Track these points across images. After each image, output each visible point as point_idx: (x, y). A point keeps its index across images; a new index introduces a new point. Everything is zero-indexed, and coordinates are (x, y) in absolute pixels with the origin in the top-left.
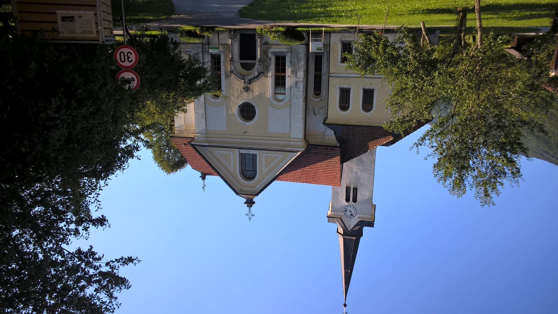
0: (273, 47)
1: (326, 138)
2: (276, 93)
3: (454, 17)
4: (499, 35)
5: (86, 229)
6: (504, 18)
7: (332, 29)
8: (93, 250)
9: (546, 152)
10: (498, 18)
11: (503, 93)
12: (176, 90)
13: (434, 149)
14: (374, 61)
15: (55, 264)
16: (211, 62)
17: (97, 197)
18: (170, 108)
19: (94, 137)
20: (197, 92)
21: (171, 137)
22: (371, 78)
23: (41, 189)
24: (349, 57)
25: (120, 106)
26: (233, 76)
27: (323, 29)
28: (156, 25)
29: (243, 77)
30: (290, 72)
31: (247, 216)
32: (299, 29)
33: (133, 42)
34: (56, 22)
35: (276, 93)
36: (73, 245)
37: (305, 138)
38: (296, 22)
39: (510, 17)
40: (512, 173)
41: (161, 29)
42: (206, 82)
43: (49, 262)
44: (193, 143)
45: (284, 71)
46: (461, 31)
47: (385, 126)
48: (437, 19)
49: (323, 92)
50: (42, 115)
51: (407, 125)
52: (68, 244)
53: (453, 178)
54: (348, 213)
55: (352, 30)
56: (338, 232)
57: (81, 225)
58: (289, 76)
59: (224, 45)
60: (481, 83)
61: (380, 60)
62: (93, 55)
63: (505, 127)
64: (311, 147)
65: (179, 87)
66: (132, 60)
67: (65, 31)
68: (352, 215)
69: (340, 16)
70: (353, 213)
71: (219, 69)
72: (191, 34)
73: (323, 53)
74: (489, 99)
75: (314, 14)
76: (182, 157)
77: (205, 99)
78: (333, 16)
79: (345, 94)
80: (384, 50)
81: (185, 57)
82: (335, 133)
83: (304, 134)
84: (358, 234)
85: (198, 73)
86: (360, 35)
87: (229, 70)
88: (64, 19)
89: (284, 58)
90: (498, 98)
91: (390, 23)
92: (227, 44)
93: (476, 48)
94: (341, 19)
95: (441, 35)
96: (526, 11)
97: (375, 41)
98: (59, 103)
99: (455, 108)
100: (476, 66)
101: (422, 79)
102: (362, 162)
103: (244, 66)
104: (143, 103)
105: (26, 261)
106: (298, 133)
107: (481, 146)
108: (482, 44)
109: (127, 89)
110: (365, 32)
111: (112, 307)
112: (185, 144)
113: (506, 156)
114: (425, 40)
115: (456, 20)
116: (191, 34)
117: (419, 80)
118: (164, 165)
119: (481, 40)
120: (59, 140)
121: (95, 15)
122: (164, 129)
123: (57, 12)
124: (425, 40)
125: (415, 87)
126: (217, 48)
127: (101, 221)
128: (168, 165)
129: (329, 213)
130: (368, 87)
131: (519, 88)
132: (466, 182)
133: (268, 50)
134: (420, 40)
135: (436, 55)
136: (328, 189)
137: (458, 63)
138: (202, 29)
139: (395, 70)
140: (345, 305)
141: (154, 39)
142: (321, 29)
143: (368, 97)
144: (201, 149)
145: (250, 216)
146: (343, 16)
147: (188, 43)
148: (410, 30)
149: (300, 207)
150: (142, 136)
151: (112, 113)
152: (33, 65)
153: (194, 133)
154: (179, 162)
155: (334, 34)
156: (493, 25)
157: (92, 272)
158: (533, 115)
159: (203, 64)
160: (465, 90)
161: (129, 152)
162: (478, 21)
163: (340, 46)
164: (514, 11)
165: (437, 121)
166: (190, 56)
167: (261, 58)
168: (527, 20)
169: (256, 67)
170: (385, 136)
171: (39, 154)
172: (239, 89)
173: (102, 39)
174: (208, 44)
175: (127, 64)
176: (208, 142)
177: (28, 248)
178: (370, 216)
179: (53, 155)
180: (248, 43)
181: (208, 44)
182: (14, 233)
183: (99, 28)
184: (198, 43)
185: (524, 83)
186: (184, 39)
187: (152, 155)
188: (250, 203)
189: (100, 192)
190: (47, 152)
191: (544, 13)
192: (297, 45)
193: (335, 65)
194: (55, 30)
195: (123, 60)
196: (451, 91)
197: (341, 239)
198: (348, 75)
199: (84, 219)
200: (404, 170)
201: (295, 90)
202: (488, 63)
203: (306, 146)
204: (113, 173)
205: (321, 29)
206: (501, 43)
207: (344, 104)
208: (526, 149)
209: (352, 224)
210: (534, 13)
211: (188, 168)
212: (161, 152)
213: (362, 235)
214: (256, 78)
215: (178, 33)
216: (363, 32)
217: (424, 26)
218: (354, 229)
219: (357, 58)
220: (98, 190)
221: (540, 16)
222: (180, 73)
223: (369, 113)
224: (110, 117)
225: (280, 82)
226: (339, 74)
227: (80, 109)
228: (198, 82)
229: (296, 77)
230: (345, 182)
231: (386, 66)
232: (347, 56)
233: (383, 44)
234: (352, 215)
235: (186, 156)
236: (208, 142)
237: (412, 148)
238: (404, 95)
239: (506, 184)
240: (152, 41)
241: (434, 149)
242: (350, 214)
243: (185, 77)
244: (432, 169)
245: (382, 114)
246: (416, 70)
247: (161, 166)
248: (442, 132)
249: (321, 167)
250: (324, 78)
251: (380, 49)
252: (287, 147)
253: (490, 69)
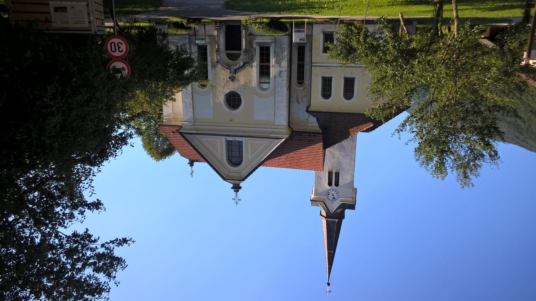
0: (258, 38)
1: (309, 125)
2: (260, 83)
3: (431, 8)
4: (475, 26)
5: (82, 213)
6: (478, 9)
7: (314, 21)
8: (89, 232)
9: (517, 137)
10: (472, 9)
11: (478, 79)
12: (164, 80)
13: (415, 134)
14: (355, 50)
15: (52, 247)
16: (198, 52)
17: (91, 182)
18: (158, 97)
19: (87, 125)
20: (183, 81)
21: (159, 125)
22: (352, 67)
23: (36, 176)
24: (331, 46)
25: (113, 95)
26: (219, 66)
27: (306, 20)
28: (144, 16)
29: (229, 67)
30: (274, 61)
31: (234, 201)
32: (283, 20)
33: (122, 32)
34: (49, 13)
35: (260, 83)
36: (66, 231)
37: (289, 126)
38: (280, 14)
39: (484, 8)
40: (490, 156)
41: (150, 21)
42: (194, 71)
43: (44, 246)
44: (181, 131)
45: (268, 61)
46: (437, 22)
47: (367, 113)
48: (414, 10)
49: (306, 82)
50: (38, 103)
51: (388, 112)
52: (66, 227)
53: (434, 161)
54: (331, 197)
55: (333, 21)
56: (321, 215)
57: (76, 209)
58: (273, 66)
59: (210, 36)
60: (457, 71)
61: (361, 49)
62: (84, 44)
63: (481, 113)
64: (295, 133)
65: (168, 77)
66: (122, 51)
67: (58, 22)
68: (334, 198)
69: (322, 8)
70: (335, 196)
71: (206, 59)
72: (178, 26)
73: (305, 43)
74: (466, 87)
75: (297, 5)
76: (171, 144)
77: (192, 89)
78: (315, 8)
79: (327, 83)
80: (365, 42)
81: (173, 48)
82: (318, 121)
83: (287, 121)
84: (341, 216)
85: (186, 63)
86: (342, 25)
87: (216, 60)
88: (56, 9)
89: (268, 49)
90: (475, 85)
91: (369, 14)
92: (213, 35)
93: (453, 37)
94: (323, 10)
95: (418, 26)
96: (499, 2)
97: (356, 31)
98: (55, 91)
99: (433, 94)
100: (453, 55)
101: (401, 67)
102: (343, 148)
103: (229, 56)
104: (132, 92)
105: (24, 245)
106: (282, 120)
107: (460, 130)
108: (458, 34)
109: (119, 77)
110: (346, 23)
111: (108, 287)
112: (173, 132)
113: (483, 140)
114: (403, 30)
115: (433, 11)
116: (178, 26)
117: (399, 69)
118: (153, 153)
119: (458, 30)
120: (54, 127)
121: (88, 5)
122: (152, 118)
123: (50, 2)
124: (403, 30)
125: (395, 75)
126: (203, 39)
127: (97, 205)
128: (158, 153)
129: (313, 196)
130: (349, 76)
131: (494, 74)
132: (446, 165)
133: (252, 41)
134: (399, 30)
135: (414, 45)
136: (311, 174)
137: (435, 52)
138: (189, 21)
139: (376, 59)
140: (329, 284)
141: (142, 31)
142: (303, 20)
143: (349, 85)
144: (189, 137)
145: (237, 201)
146: (325, 7)
147: (175, 35)
148: (390, 21)
149: (284, 191)
150: (132, 124)
151: (106, 101)
152: (29, 54)
153: (181, 121)
154: (168, 149)
155: (316, 25)
156: (468, 16)
157: (89, 253)
158: (507, 100)
159: (190, 54)
160: (443, 77)
161: (123, 140)
162: (454, 11)
163: (321, 37)
164: (488, 2)
165: (417, 107)
166: (177, 47)
167: (246, 49)
168: (500, 11)
169: (242, 57)
170: (365, 123)
171: (35, 141)
172: (225, 78)
173: (94, 29)
174: (195, 36)
175: (117, 54)
176: (195, 129)
177: (24, 233)
178: (351, 199)
179: (48, 142)
180: (233, 34)
181: (195, 36)
182: (11, 219)
183: (91, 18)
184: (185, 35)
185: (499, 70)
186: (171, 31)
187: (141, 143)
188: (237, 188)
189: (94, 178)
190: (43, 138)
191: (515, 4)
192: (281, 36)
193: (317, 55)
194: (48, 21)
195: (113, 50)
196: (430, 79)
197: (324, 221)
198: (330, 65)
199: (79, 204)
200: (386, 154)
201: (280, 79)
202: (464, 52)
203: (290, 133)
204: (108, 160)
205: (303, 20)
206: (477, 32)
207: (326, 93)
208: (502, 133)
209: (334, 207)
210: (506, 4)
211: (176, 155)
212: (150, 140)
213: (344, 218)
214: (241, 67)
215: (166, 24)
216: (344, 23)
217: (402, 17)
218: (336, 212)
219: (340, 48)
220: (91, 176)
221: (512, 7)
222: (168, 64)
223: (350, 101)
224: (104, 104)
225: (264, 71)
226: (321, 63)
227: (75, 97)
228: (186, 72)
229: (280, 66)
230: (327, 168)
231: (367, 56)
232: (329, 46)
233: (364, 34)
234: (334, 198)
235: (175, 144)
236: (195, 129)
237: (393, 134)
238: (385, 83)
239: (486, 166)
240: (140, 33)
241: (415, 134)
242: (332, 197)
243: (174, 67)
244: (413, 153)
245: (363, 101)
246: (396, 59)
247: (150, 154)
248: (422, 118)
249: (304, 153)
250: (307, 68)
251: (361, 39)
252: (271, 134)
253: (467, 57)
